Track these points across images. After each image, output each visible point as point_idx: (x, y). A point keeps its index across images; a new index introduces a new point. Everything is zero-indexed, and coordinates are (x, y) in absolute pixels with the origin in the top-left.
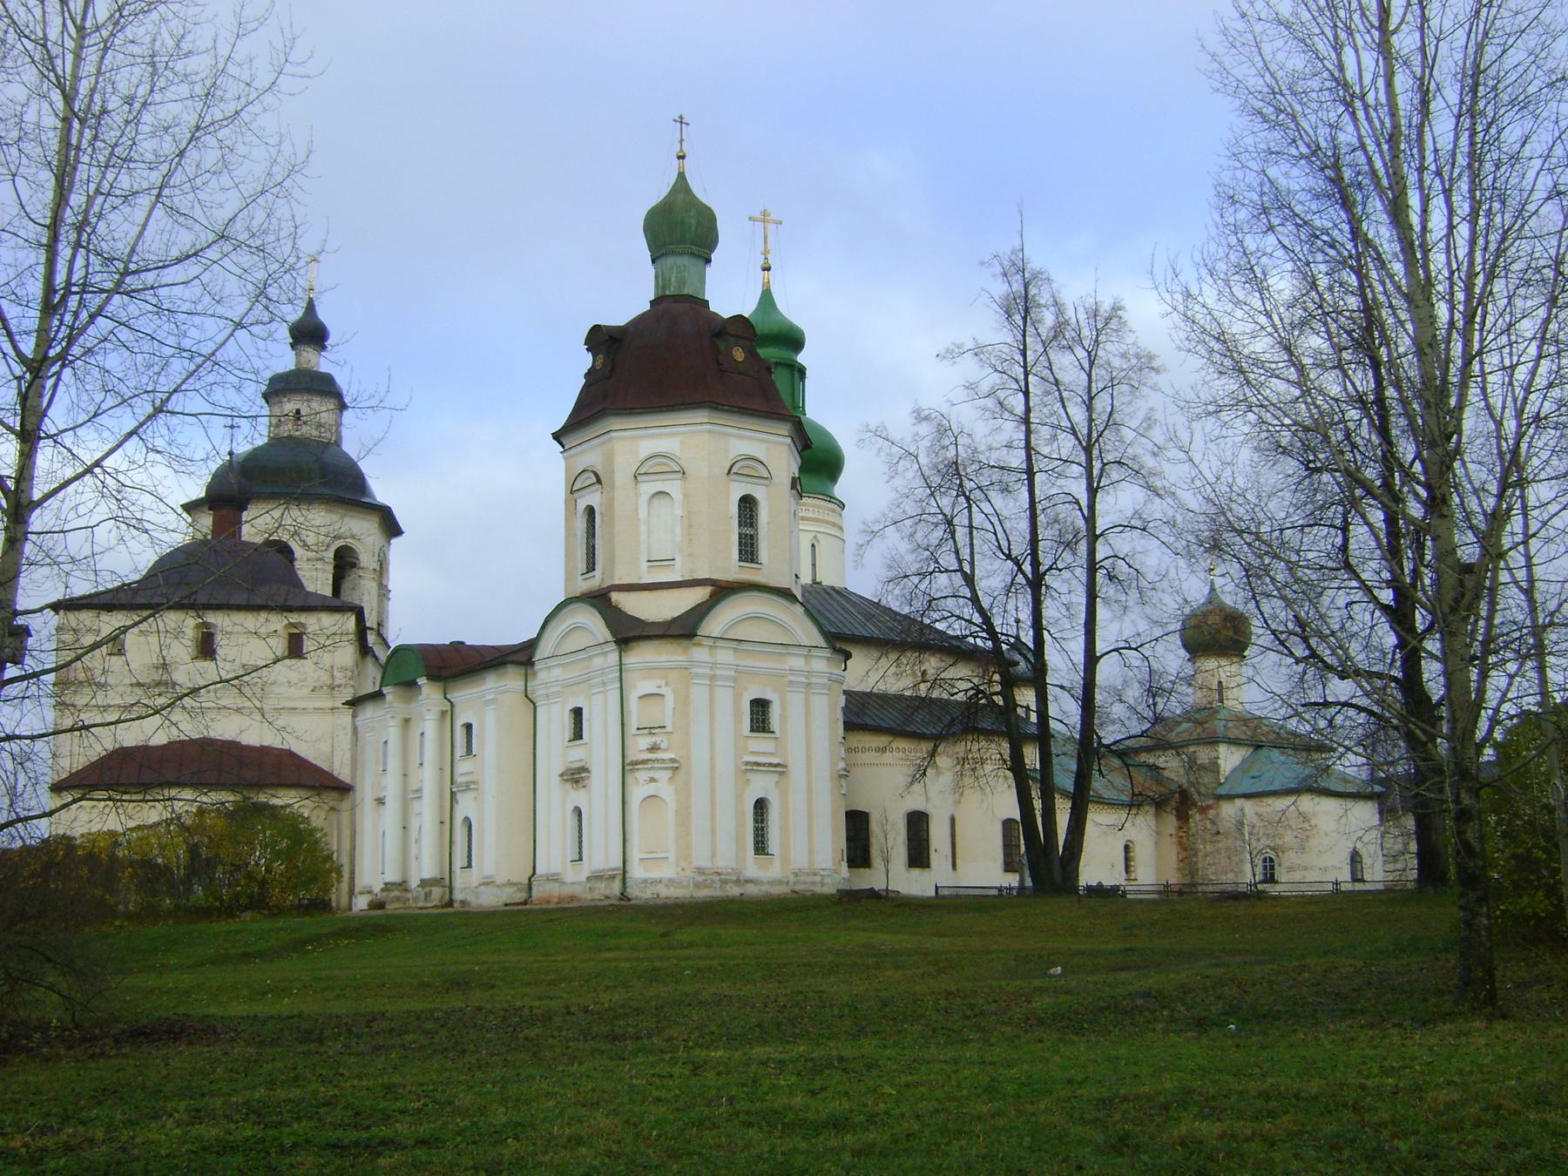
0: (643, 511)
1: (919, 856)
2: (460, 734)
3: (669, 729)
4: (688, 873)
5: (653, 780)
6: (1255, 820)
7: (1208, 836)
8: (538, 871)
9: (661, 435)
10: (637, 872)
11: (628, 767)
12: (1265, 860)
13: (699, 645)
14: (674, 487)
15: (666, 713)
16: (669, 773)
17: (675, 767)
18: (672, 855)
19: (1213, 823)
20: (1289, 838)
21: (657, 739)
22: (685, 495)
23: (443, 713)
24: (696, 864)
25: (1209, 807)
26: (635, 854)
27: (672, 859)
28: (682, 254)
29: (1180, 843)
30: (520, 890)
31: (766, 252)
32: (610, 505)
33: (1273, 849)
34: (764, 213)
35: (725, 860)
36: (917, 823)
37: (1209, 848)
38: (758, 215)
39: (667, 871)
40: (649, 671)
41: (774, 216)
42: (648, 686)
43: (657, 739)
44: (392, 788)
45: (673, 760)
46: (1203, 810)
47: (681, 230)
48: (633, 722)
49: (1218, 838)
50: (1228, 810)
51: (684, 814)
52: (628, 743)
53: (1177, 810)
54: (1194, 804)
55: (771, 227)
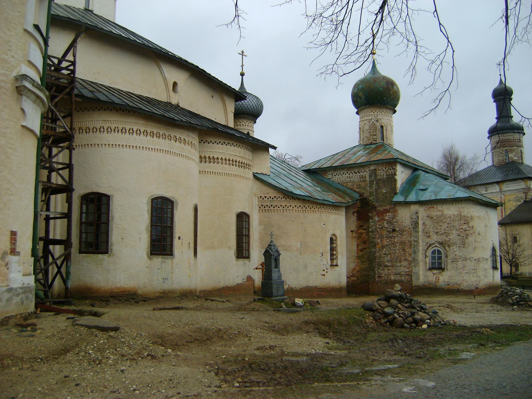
1: (161, 243)
6: (428, 222)
7: (385, 233)
12: (434, 252)
19: (389, 222)
20: (453, 236)
25: (387, 211)
31: (242, 66)
34: (243, 52)
36: (162, 210)
44: (509, 244)
46: (381, 214)
49: (395, 234)
53: (358, 212)
54: (374, 208)
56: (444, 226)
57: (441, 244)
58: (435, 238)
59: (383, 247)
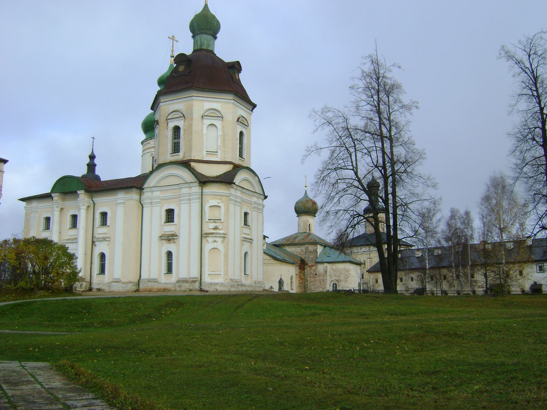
0: (205, 131)
2: (98, 217)
3: (222, 221)
4: (228, 281)
5: (215, 241)
6: (331, 271)
7: (312, 275)
8: (142, 277)
9: (213, 101)
10: (207, 279)
11: (203, 236)
12: (333, 284)
13: (233, 188)
14: (218, 123)
15: (221, 214)
16: (222, 239)
17: (224, 237)
18: (222, 273)
19: (314, 271)
20: (342, 277)
21: (217, 224)
22: (223, 127)
23: (88, 207)
24: (230, 277)
25: (313, 266)
26: (206, 271)
27: (222, 275)
28: (210, 34)
29: (300, 277)
30: (134, 285)
32: (190, 128)
33: (337, 281)
34: (173, 37)
35: (236, 277)
37: (312, 279)
38: (171, 37)
39: (220, 280)
40: (215, 195)
41: (176, 39)
42: (214, 202)
43: (217, 224)
45: (224, 234)
47: (205, 25)
48: (207, 217)
50: (320, 268)
51: (226, 256)
52: (95, 229)
54: (307, 264)
55: (175, 42)
56: (338, 273)
57: (337, 281)
58: (334, 278)
59: (311, 282)
